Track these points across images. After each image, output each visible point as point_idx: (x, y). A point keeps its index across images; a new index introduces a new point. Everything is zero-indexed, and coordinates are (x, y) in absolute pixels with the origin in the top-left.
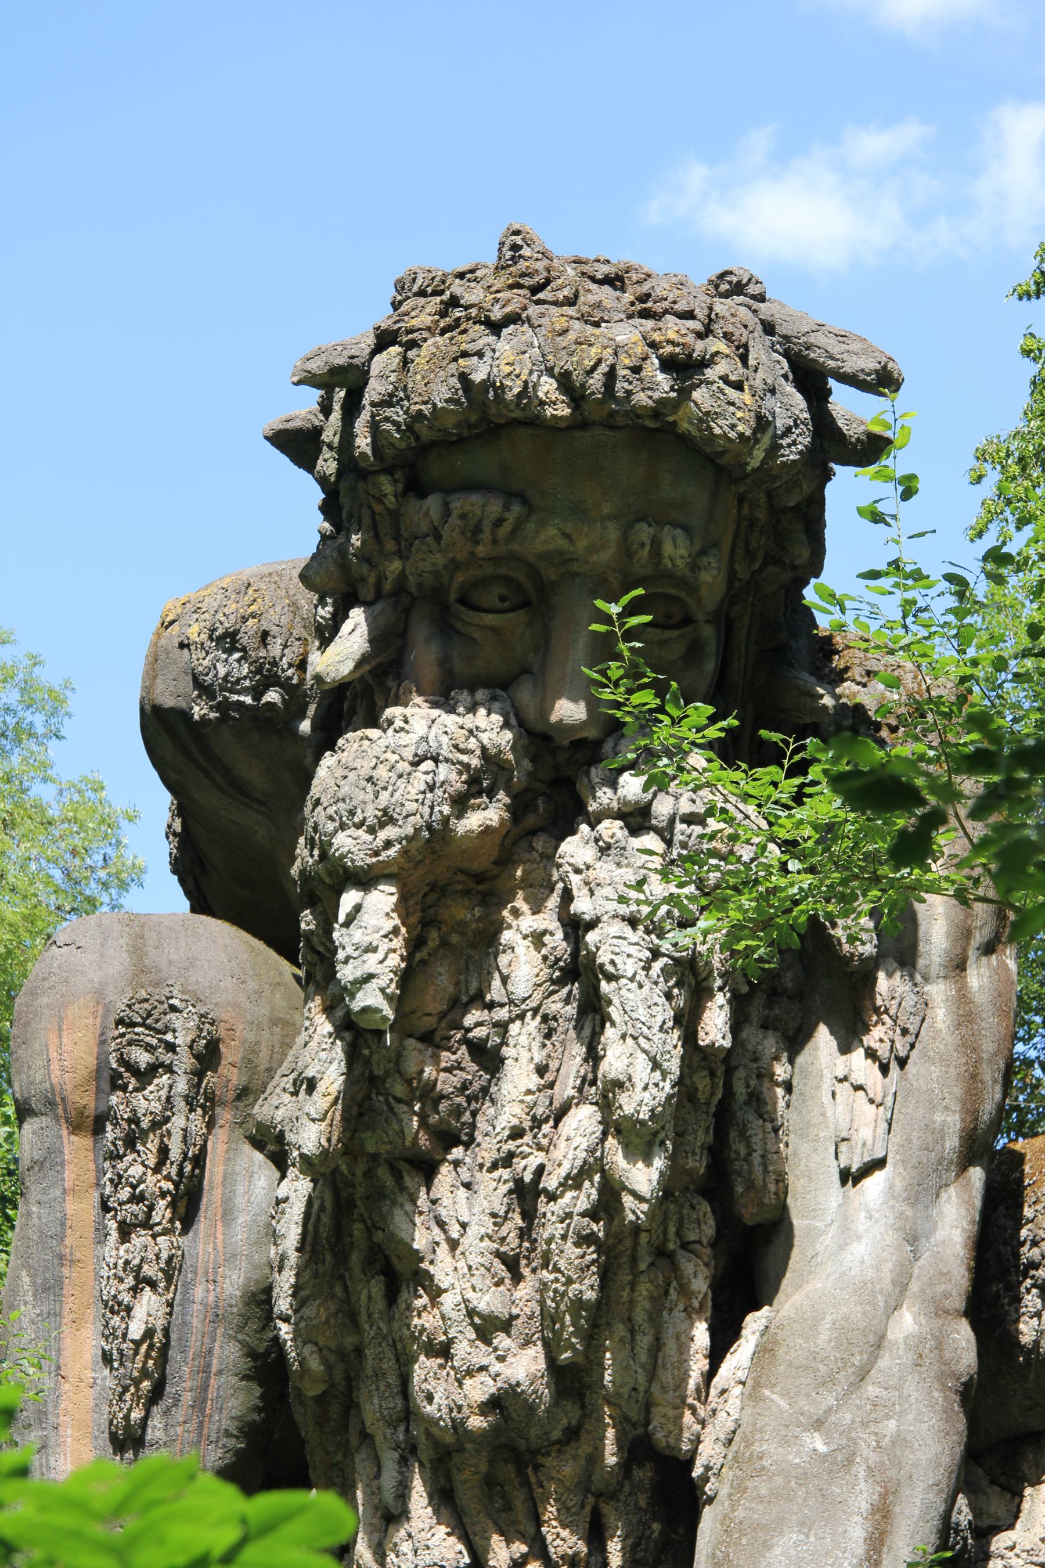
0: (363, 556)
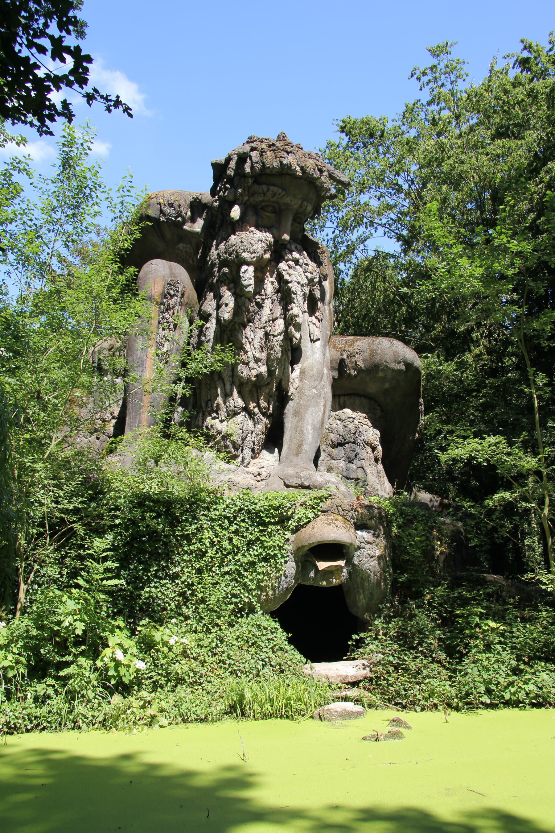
0: (241, 194)
